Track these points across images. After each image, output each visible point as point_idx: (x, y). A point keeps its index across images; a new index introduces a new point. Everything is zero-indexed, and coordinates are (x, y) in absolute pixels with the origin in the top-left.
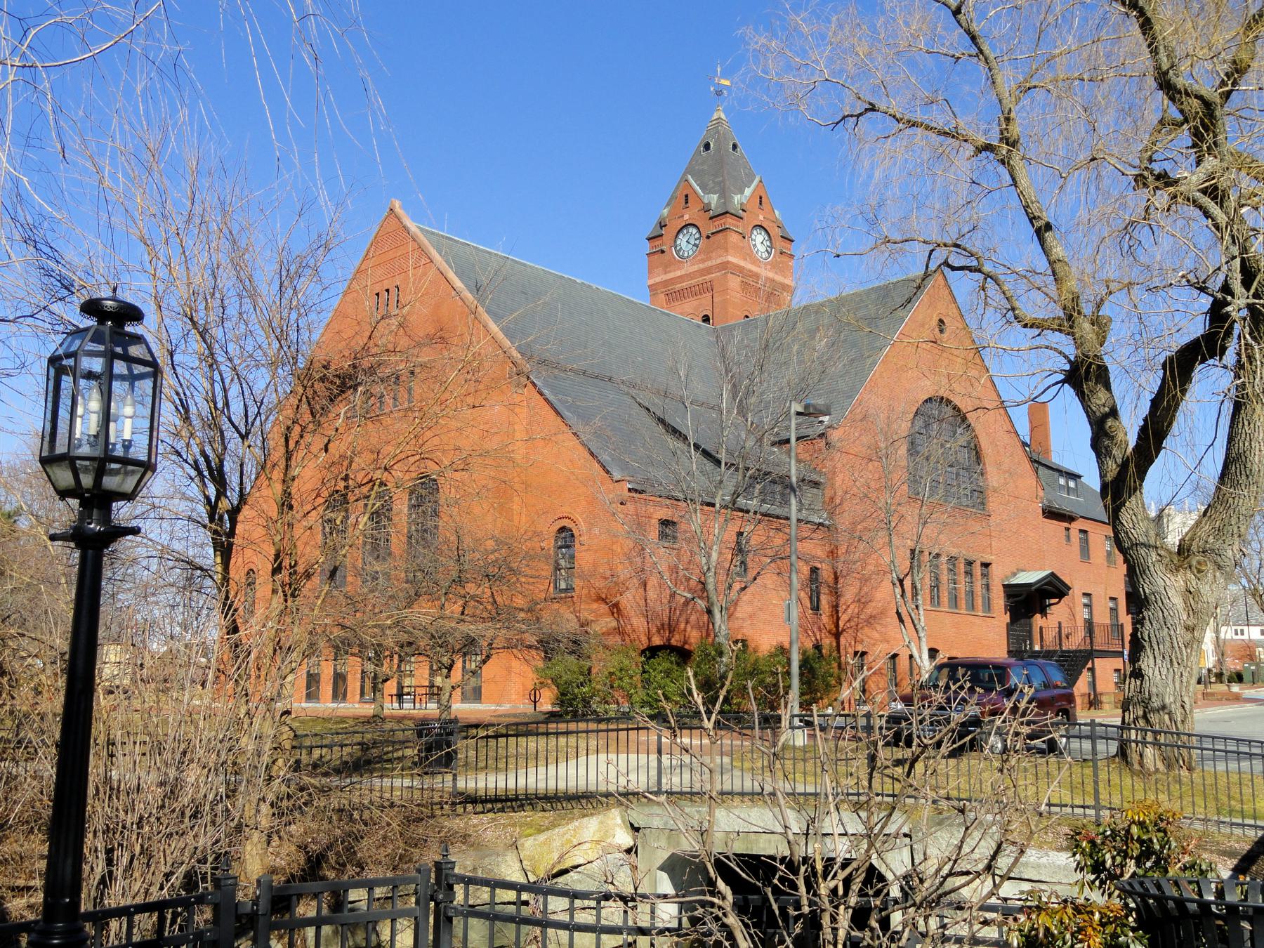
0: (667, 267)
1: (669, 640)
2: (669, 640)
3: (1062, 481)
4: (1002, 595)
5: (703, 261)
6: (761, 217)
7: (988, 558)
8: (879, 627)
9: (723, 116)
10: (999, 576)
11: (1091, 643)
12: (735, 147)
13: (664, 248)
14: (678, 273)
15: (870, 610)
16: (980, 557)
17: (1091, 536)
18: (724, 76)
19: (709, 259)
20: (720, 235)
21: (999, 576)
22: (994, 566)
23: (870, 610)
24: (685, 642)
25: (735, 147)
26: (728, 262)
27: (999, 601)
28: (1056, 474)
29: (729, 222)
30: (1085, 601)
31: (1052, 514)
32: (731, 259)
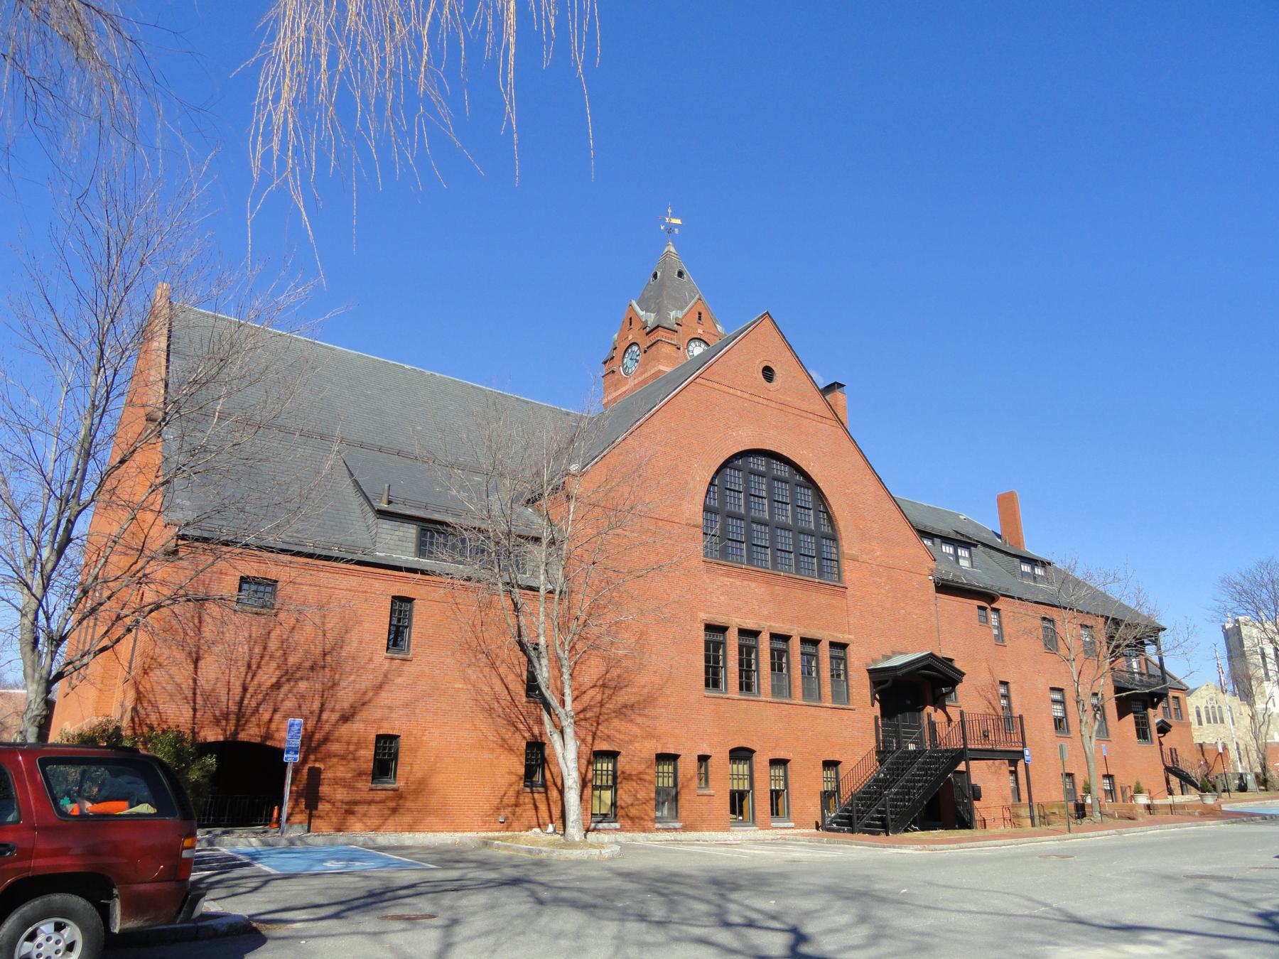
0: (616, 386)
1: (236, 733)
2: (236, 733)
3: (1026, 568)
4: (867, 681)
5: (641, 374)
6: (700, 331)
7: (840, 637)
8: (639, 720)
9: (672, 249)
10: (860, 661)
11: (964, 738)
12: (680, 274)
13: (615, 368)
14: (624, 389)
15: (622, 698)
16: (826, 636)
17: (1059, 628)
18: (673, 216)
19: (646, 371)
20: (654, 348)
21: (860, 661)
22: (852, 650)
23: (622, 698)
24: (268, 736)
25: (680, 274)
26: (660, 371)
27: (861, 687)
28: (1017, 561)
29: (660, 334)
30: (1002, 691)
31: (945, 588)
32: (661, 368)
